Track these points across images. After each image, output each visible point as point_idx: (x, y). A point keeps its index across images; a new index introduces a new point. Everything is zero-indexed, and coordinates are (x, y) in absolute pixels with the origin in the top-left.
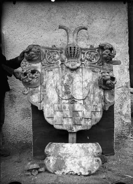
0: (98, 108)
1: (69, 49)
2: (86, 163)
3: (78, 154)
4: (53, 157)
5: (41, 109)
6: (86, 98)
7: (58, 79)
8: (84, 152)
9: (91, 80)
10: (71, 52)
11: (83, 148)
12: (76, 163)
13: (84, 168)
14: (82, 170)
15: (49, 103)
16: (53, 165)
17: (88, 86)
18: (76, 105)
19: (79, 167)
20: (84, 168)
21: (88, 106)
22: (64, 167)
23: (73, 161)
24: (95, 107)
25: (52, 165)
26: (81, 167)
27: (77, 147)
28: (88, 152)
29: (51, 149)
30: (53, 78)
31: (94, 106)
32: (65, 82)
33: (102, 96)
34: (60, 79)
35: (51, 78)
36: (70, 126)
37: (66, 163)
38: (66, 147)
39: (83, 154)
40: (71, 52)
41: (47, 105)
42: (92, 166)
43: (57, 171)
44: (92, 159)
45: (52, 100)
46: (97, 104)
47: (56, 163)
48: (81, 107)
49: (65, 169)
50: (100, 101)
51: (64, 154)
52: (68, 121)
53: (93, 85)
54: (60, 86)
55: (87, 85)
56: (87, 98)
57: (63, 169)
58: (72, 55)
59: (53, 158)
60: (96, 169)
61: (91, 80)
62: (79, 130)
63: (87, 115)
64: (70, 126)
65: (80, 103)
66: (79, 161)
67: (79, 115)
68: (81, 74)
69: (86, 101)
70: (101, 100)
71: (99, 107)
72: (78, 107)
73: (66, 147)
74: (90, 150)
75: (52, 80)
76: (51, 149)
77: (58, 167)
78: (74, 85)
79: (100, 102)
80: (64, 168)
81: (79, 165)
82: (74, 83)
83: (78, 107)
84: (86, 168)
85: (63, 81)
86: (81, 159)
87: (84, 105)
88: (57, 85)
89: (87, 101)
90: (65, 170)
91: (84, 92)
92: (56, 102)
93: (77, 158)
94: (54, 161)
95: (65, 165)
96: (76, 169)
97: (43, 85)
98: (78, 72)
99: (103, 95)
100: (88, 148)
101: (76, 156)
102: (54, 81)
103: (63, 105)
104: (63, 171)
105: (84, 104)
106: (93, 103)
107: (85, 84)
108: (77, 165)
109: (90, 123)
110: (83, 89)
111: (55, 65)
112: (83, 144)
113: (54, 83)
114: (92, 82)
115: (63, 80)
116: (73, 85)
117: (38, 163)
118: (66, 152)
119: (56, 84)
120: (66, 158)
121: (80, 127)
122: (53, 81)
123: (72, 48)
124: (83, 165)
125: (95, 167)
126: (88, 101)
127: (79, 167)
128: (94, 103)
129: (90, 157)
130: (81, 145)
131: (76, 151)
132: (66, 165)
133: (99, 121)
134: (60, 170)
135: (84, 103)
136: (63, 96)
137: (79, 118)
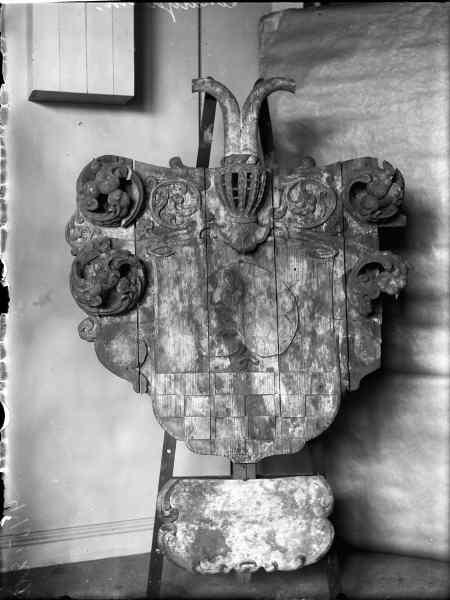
0: (328, 384)
1: (228, 179)
2: (287, 535)
3: (265, 509)
4: (184, 524)
5: (98, 298)
6: (286, 352)
7: (194, 285)
8: (282, 504)
9: (304, 288)
10: (235, 193)
11: (360, 374)
12: (259, 539)
13: (284, 551)
14: (277, 557)
15: (166, 371)
16: (187, 548)
17: (293, 310)
18: (256, 374)
19: (267, 548)
20: (284, 551)
21: (295, 378)
22: (222, 550)
23: (249, 533)
24: (315, 381)
25: (183, 547)
26: (275, 547)
27: (260, 490)
28: (294, 505)
29: (178, 500)
30: (177, 280)
31: (314, 376)
32: (217, 298)
33: (340, 341)
34: (200, 286)
35: (172, 281)
36: (239, 445)
37: (227, 540)
38: (224, 493)
39: (279, 512)
40: (235, 193)
41: (162, 375)
42: (307, 543)
43: (202, 565)
44: (307, 524)
45: (178, 359)
46: (322, 370)
47: (197, 541)
48: (271, 381)
49: (224, 555)
50: (332, 359)
51: (223, 514)
52: (231, 428)
53: (310, 304)
54: (202, 310)
55: (291, 306)
56: (292, 350)
57: (220, 557)
58: (241, 204)
59: (187, 526)
60: (317, 549)
61: (304, 288)
62: (265, 456)
63: (292, 406)
64: (239, 445)
65: (269, 366)
66: (267, 532)
67: (265, 408)
68: (272, 266)
69: (287, 359)
70: (335, 356)
71: (330, 381)
72: (262, 382)
73: (224, 493)
74: (299, 497)
75: (174, 287)
76: (178, 500)
77: (205, 552)
78: (248, 306)
79: (331, 363)
80: (221, 554)
81: (267, 542)
82: (247, 300)
83: (262, 382)
84: (290, 549)
85: (212, 293)
86: (274, 525)
87: (282, 375)
88: (191, 306)
89: (292, 361)
90: (227, 560)
91: (281, 329)
92: (191, 367)
93: (261, 523)
94: (189, 535)
95: (226, 546)
96: (264, 558)
97: (144, 308)
98: (261, 260)
99: (344, 340)
100: (292, 492)
101: (259, 519)
102: (181, 293)
103: (212, 375)
104: (220, 561)
105: (283, 372)
106: (310, 366)
107: (284, 303)
108: (263, 543)
109: (300, 431)
110: (280, 320)
111: (183, 234)
112: (276, 480)
113: (182, 300)
114: (309, 294)
115: (211, 289)
116: (244, 304)
117: (27, 520)
118: (225, 509)
119: (187, 304)
120: (226, 523)
121: (269, 444)
122: (176, 293)
123: (240, 179)
124: (281, 543)
125: (315, 546)
126: (295, 361)
127: (269, 547)
128: (315, 365)
129: (300, 517)
130: (269, 484)
131: (259, 503)
132: (229, 545)
133: (327, 426)
134: (211, 559)
135: (283, 368)
136: (212, 345)
137: (267, 418)
